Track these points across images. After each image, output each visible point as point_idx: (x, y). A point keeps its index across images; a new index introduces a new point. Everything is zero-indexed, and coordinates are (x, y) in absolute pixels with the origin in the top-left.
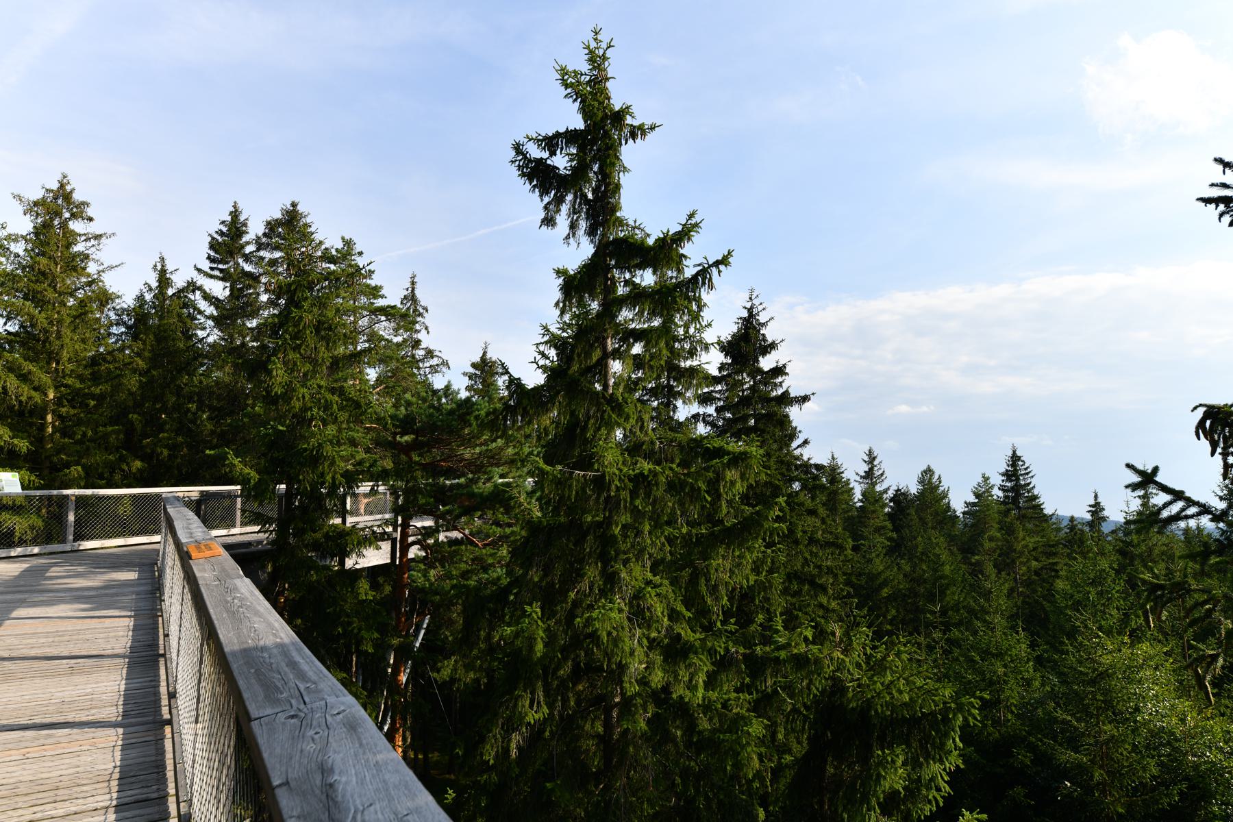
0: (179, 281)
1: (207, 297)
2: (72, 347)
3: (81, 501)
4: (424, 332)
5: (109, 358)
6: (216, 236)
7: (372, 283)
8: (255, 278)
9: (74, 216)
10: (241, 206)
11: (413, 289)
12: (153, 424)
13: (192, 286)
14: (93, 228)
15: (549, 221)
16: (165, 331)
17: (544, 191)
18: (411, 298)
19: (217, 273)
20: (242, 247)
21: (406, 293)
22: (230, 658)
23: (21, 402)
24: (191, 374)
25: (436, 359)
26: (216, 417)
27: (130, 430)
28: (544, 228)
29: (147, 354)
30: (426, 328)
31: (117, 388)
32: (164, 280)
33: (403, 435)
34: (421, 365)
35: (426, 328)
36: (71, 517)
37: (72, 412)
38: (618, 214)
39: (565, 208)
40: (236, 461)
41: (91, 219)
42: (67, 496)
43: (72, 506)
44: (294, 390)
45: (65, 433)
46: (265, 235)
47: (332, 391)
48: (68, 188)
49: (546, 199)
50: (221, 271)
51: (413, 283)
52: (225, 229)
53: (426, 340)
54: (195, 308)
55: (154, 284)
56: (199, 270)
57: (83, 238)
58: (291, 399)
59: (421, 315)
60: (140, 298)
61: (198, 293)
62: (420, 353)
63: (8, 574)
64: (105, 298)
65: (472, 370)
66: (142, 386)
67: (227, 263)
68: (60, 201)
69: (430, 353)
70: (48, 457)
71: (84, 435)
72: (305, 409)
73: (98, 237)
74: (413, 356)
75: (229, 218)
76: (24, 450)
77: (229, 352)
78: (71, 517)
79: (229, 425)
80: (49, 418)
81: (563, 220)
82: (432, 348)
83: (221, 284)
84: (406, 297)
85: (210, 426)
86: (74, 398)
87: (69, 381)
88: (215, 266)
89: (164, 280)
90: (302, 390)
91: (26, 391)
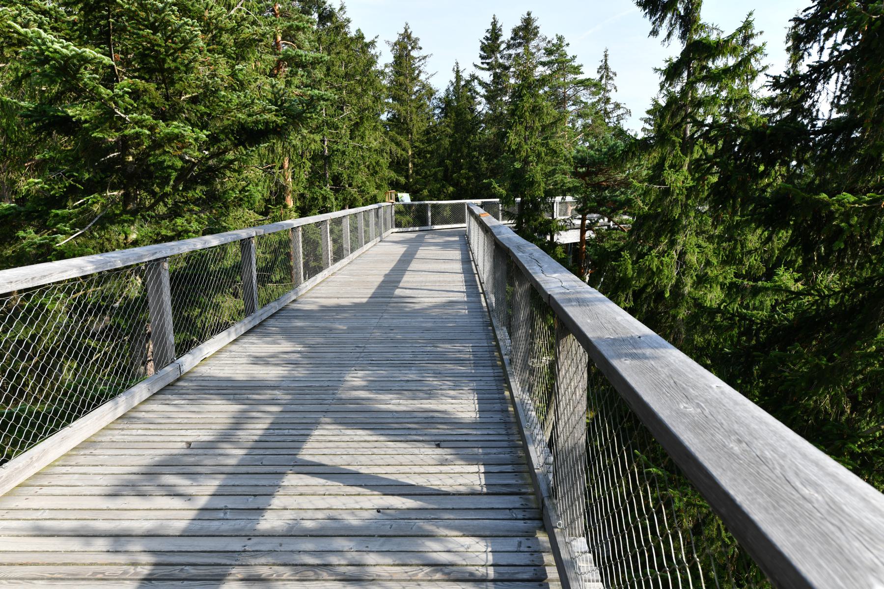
0: (466, 76)
1: (481, 83)
2: (418, 126)
3: (434, 206)
4: (613, 90)
5: (434, 130)
6: (484, 41)
7: (575, 64)
8: (507, 68)
9: (413, 48)
10: (497, 18)
11: (606, 60)
12: (458, 166)
13: (474, 77)
14: (422, 53)
15: (654, 33)
16: (460, 110)
17: (652, 13)
18: (605, 67)
19: (485, 66)
20: (499, 46)
21: (601, 64)
22: (564, 563)
23: (397, 157)
24: (475, 135)
25: (621, 109)
26: (489, 160)
27: (446, 170)
28: (651, 37)
29: (452, 125)
30: (615, 88)
31: (439, 147)
32: (458, 77)
33: (581, 167)
34: (611, 116)
35: (615, 88)
36: (430, 214)
37: (420, 161)
38: (701, 22)
39: (666, 21)
40: (496, 186)
41: (421, 48)
42: (427, 204)
43: (430, 209)
44: (521, 147)
45: (417, 173)
46: (512, 38)
47: (542, 145)
48: (409, 31)
49: (654, 19)
50: (488, 64)
51: (606, 56)
52: (489, 35)
53: (614, 97)
54: (475, 92)
55: (454, 80)
56: (475, 66)
57: (418, 60)
58: (520, 151)
59: (611, 78)
60: (448, 90)
61: (476, 81)
62: (610, 107)
63: (32, 573)
64: (431, 93)
65: (647, 116)
66: (451, 144)
67: (491, 58)
68: (406, 40)
69: (617, 106)
70: (411, 186)
71: (426, 173)
72: (527, 157)
73: (424, 58)
74: (605, 110)
75: (491, 27)
76: (404, 183)
77: (494, 119)
78: (430, 214)
79: (495, 164)
80: (410, 165)
81: (663, 31)
82: (618, 102)
83: (488, 73)
84: (601, 67)
85: (485, 166)
86: (419, 153)
87: (417, 144)
88: (484, 61)
89: (458, 77)
90: (526, 146)
91: (400, 152)
